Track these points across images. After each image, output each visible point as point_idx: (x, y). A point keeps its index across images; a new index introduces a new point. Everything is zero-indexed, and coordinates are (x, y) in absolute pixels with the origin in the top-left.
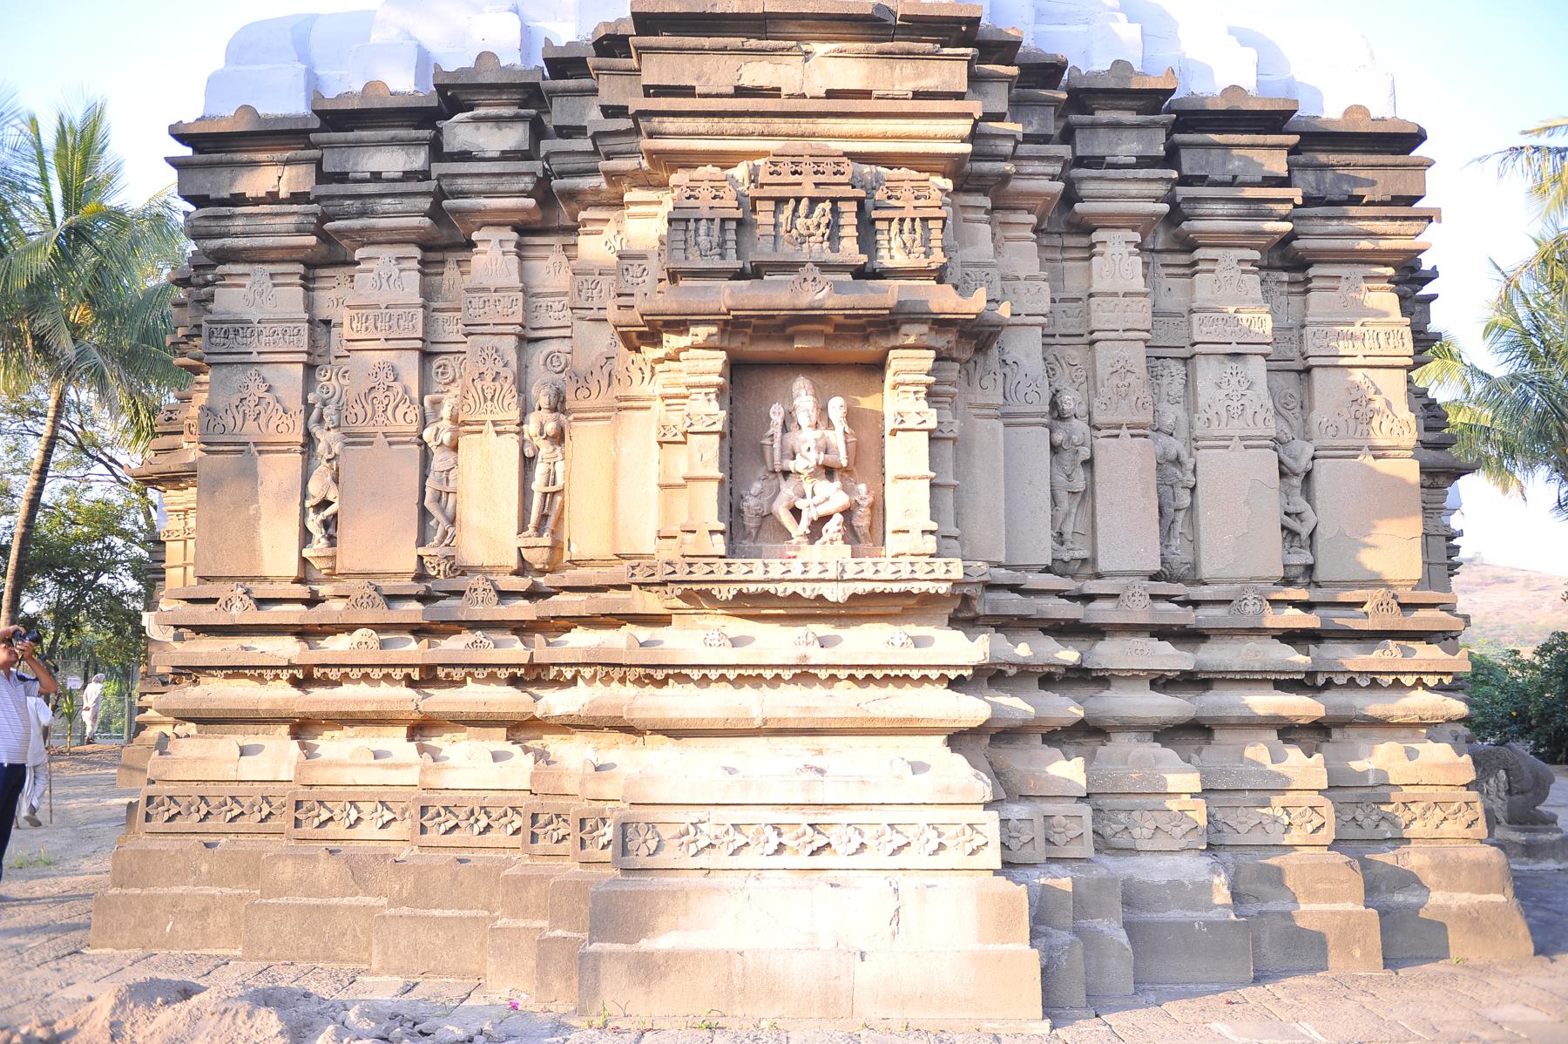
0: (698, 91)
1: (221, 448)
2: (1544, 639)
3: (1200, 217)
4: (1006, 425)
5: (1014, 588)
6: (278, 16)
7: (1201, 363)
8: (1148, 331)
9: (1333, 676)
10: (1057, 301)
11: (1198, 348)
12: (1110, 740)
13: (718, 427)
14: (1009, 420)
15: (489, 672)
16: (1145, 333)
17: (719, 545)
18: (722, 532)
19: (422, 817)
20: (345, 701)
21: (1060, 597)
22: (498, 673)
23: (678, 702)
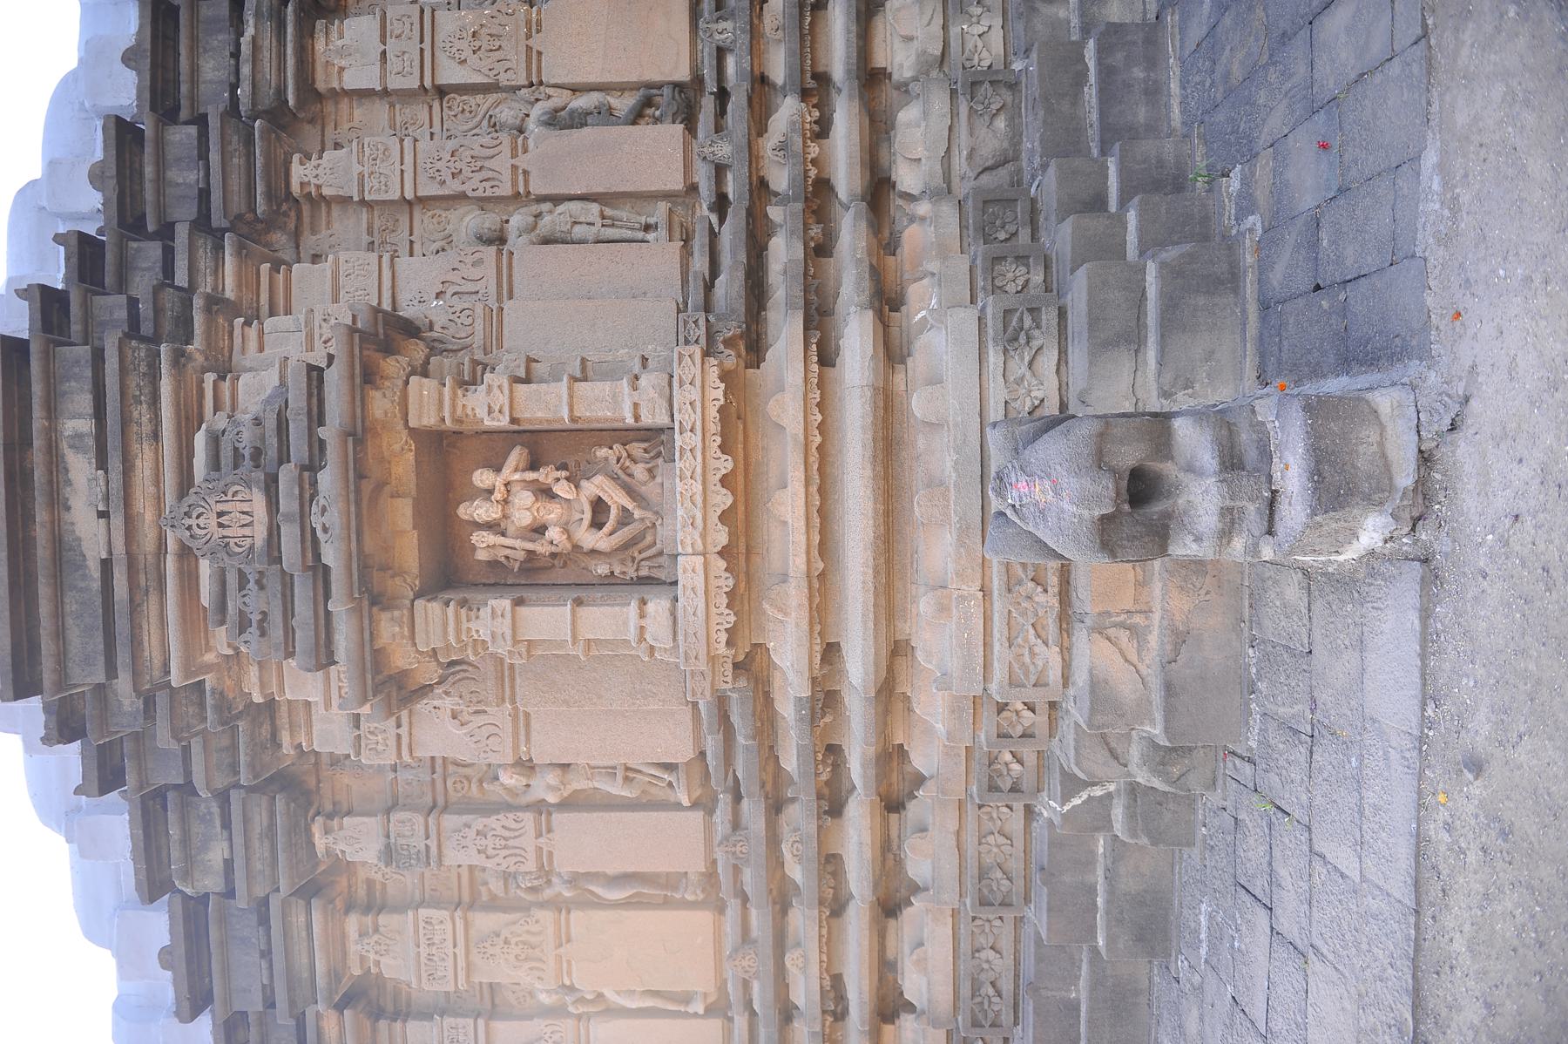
0: (104, 555)
1: (534, 66)
2: (766, 179)
3: (281, 91)
4: (511, 297)
5: (709, 287)
6: (3, 507)
7: (441, 80)
8: (402, 141)
9: (810, 157)
10: (371, 239)
11: (428, 83)
12: (907, 642)
13: (505, 604)
14: (505, 292)
15: (830, 945)
16: (405, 143)
17: (658, 606)
18: (643, 602)
19: (1024, 686)
20: (865, 776)
21: (713, 285)
22: (813, 155)
23: (858, 669)
